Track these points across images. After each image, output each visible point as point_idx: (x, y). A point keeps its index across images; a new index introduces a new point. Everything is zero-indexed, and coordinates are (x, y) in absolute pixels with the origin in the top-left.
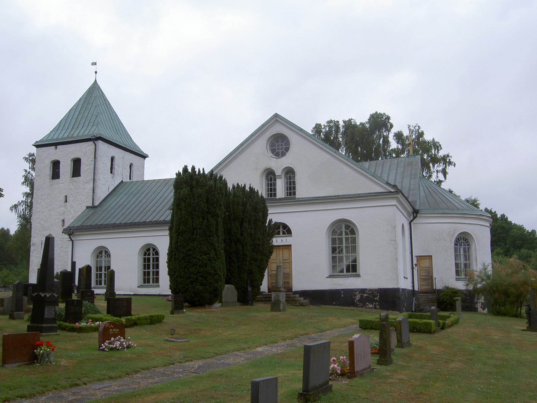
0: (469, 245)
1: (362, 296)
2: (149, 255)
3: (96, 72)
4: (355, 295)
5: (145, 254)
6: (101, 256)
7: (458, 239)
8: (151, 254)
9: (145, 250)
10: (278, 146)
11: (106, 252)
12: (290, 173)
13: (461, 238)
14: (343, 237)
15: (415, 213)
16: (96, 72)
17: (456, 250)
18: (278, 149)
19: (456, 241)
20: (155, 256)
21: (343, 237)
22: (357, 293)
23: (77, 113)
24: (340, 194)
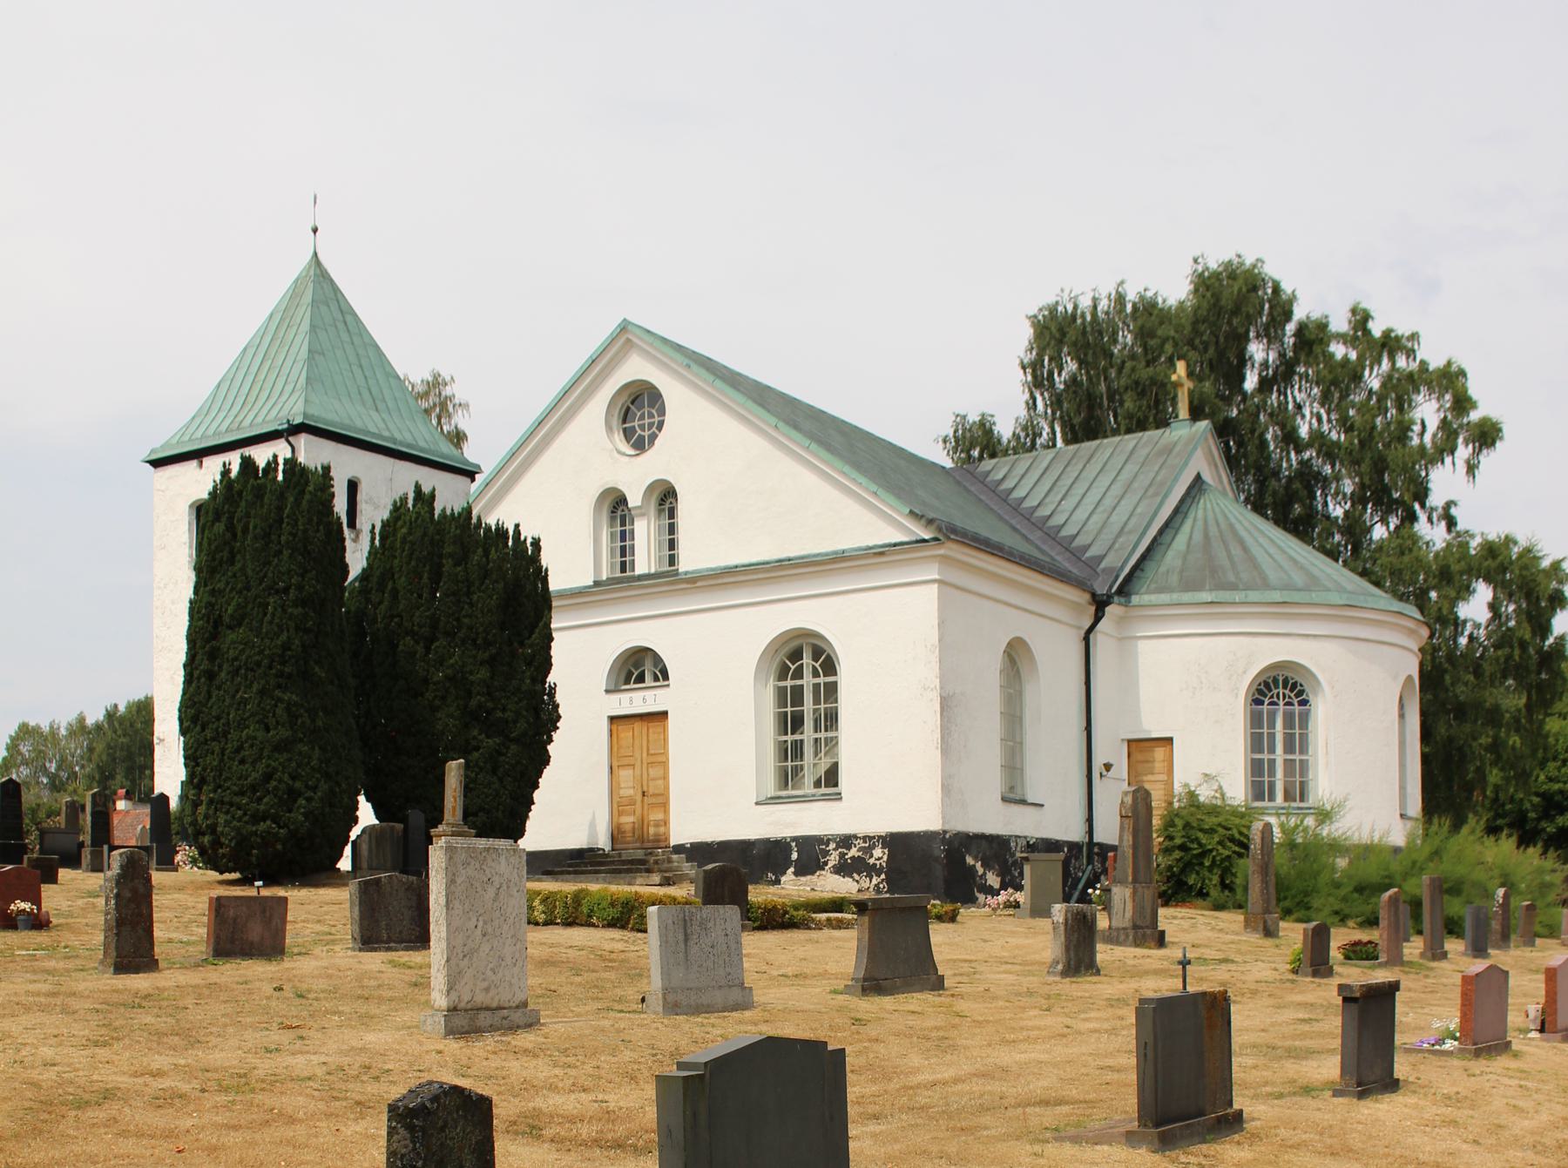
0: (1304, 703)
1: (842, 855)
2: (798, 674)
3: (315, 231)
4: (827, 853)
5: (783, 673)
6: (800, 669)
7: (1267, 684)
8: (807, 672)
9: (782, 656)
10: (642, 417)
11: (817, 653)
12: (665, 497)
13: (1275, 681)
14: (803, 680)
15: (1100, 605)
16: (315, 231)
17: (1255, 720)
18: (642, 427)
19: (1260, 692)
20: (821, 680)
21: (803, 680)
22: (832, 846)
23: (268, 339)
24: (792, 555)
